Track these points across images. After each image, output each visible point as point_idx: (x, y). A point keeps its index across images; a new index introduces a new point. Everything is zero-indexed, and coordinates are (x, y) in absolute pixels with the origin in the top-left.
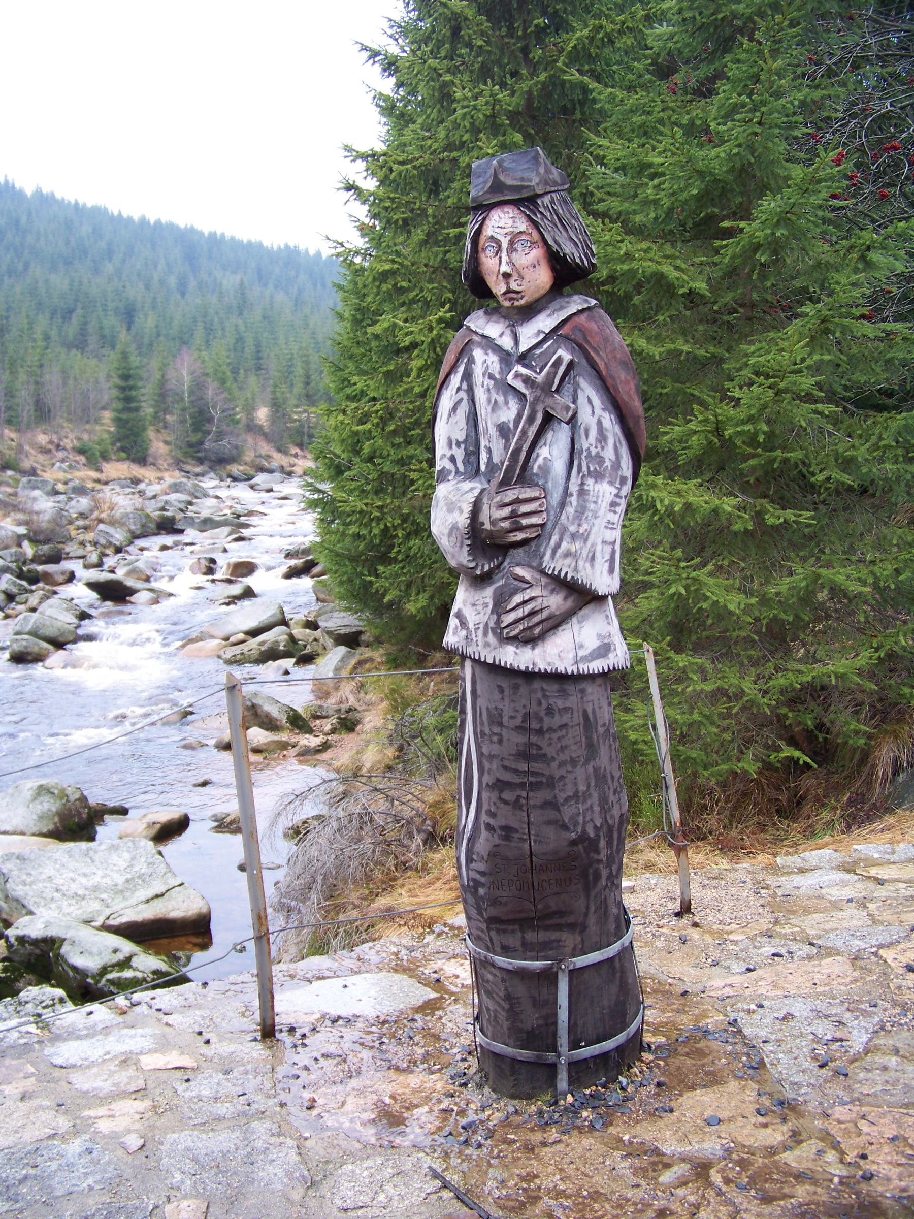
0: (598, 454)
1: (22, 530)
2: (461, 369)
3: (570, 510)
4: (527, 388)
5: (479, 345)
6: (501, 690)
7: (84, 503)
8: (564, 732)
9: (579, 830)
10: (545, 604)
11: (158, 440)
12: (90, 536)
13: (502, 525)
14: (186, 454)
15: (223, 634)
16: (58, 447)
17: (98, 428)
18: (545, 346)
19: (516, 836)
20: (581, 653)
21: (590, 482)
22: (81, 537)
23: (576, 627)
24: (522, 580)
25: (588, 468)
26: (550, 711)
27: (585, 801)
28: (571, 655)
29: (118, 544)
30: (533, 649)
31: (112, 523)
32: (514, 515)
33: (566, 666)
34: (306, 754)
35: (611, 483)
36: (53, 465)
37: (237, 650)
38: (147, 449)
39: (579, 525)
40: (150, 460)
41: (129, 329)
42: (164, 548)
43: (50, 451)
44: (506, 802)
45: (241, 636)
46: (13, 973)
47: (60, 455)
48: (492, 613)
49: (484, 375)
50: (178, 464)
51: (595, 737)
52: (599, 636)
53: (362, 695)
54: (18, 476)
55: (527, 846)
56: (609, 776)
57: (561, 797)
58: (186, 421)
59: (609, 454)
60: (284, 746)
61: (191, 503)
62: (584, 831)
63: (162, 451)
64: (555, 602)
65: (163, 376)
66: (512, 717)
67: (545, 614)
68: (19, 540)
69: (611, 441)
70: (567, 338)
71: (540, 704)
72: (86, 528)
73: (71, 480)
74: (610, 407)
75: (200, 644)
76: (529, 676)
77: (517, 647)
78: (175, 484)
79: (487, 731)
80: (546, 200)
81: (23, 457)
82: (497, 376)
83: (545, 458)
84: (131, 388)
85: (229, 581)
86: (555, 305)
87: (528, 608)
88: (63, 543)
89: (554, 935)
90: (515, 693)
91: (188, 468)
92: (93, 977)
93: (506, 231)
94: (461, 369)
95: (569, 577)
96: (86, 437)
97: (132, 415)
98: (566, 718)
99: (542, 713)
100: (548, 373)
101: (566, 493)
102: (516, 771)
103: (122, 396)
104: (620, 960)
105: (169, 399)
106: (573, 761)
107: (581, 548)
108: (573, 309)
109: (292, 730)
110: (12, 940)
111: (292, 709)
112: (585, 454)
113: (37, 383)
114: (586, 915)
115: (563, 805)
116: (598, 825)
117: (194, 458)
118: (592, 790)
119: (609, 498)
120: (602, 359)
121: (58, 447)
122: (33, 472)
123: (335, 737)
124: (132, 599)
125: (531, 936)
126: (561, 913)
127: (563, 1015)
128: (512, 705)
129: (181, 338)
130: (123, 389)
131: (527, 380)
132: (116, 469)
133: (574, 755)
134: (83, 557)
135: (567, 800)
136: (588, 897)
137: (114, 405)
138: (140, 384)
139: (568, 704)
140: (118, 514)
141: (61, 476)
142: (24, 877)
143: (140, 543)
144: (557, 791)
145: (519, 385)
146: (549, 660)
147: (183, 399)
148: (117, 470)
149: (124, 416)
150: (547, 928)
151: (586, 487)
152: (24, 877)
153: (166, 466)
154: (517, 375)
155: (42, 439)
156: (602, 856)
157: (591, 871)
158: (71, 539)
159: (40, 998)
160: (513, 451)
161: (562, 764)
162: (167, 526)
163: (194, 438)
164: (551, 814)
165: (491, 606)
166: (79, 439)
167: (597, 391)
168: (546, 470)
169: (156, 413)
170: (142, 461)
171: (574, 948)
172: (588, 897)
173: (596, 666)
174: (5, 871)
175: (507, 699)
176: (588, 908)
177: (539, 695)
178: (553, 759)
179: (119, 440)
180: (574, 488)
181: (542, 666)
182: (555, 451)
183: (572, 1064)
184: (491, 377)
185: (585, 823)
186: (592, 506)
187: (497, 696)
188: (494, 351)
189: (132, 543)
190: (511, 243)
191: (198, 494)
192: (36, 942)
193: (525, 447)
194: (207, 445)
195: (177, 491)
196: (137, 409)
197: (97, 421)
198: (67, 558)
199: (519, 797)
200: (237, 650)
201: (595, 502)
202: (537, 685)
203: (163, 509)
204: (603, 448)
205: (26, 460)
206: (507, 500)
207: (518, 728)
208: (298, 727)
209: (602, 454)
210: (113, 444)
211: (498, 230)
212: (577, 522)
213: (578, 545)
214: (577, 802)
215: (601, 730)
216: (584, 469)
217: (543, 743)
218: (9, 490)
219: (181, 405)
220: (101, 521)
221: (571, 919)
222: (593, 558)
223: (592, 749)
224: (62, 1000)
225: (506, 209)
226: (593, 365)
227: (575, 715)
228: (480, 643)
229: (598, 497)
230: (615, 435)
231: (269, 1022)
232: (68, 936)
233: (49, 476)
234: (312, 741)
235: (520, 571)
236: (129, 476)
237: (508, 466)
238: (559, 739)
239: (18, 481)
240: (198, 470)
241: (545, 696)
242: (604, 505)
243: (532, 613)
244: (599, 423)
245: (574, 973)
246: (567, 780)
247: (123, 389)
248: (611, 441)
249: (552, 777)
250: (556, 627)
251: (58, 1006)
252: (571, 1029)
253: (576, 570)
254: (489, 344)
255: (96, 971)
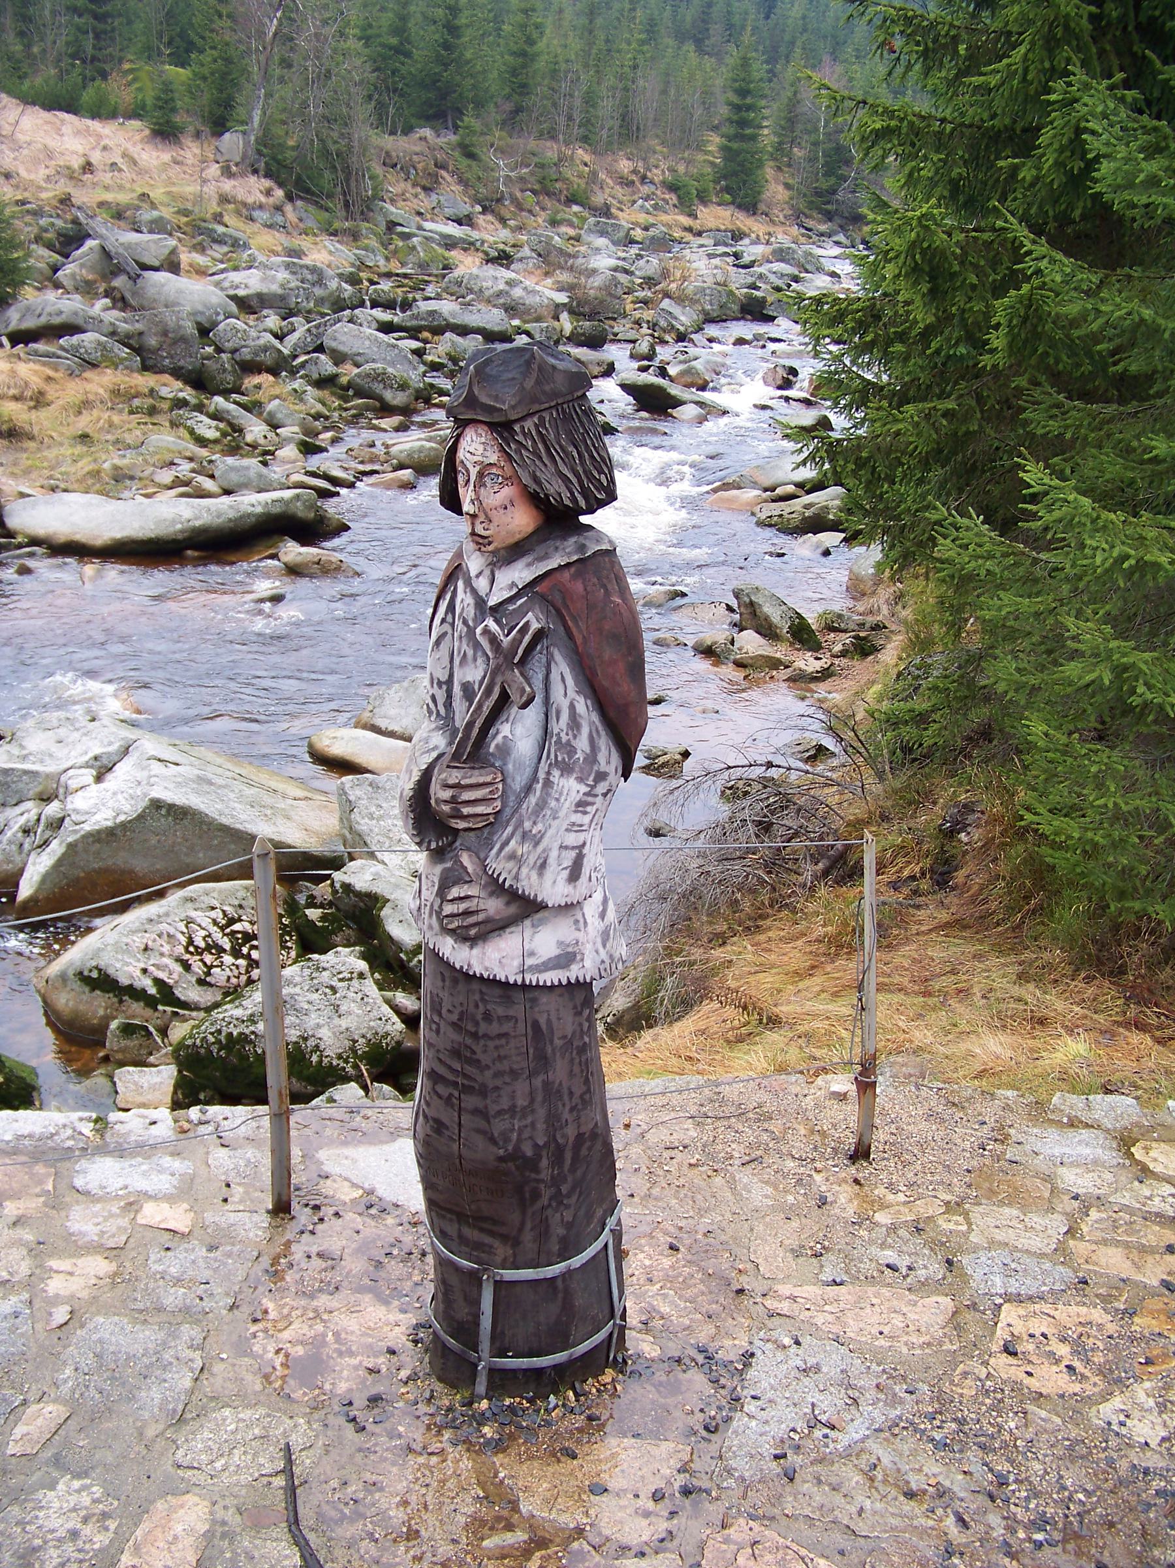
0: (568, 743)
1: (562, 298)
2: (448, 596)
3: (533, 800)
7: (651, 264)
8: (503, 1041)
9: (510, 1148)
10: (482, 906)
11: (777, 181)
12: (648, 315)
14: (811, 205)
15: (768, 483)
16: (643, 178)
17: (700, 157)
18: (519, 602)
20: (530, 962)
21: (556, 773)
22: (637, 314)
23: (528, 933)
26: (487, 1017)
27: (524, 1116)
28: (516, 963)
29: (682, 329)
30: (471, 948)
31: (681, 299)
32: (453, 800)
33: (508, 972)
34: (800, 680)
35: (580, 780)
36: (635, 202)
37: (776, 509)
38: (759, 193)
40: (762, 207)
41: (767, 17)
42: (740, 342)
43: (633, 182)
44: (440, 1097)
45: (791, 489)
46: (332, 923)
47: (646, 189)
50: (797, 217)
51: (549, 1050)
52: (560, 943)
53: (899, 607)
54: (586, 214)
55: (455, 1146)
56: (565, 1091)
57: (493, 1108)
58: (817, 159)
59: (582, 744)
60: (775, 664)
61: (796, 279)
62: (517, 1148)
63: (780, 197)
64: (493, 906)
65: (795, 93)
67: (481, 917)
68: (557, 309)
69: (585, 731)
70: (544, 598)
71: (477, 1006)
72: (645, 302)
73: (653, 225)
74: (588, 690)
75: (734, 493)
76: (466, 977)
78: (781, 250)
80: (529, 424)
81: (596, 188)
83: (505, 737)
84: (749, 108)
85: (807, 403)
86: (540, 550)
87: (463, 906)
88: (614, 319)
89: (487, 1239)
91: (810, 223)
92: (407, 953)
93: (476, 458)
94: (448, 596)
95: (507, 885)
96: (681, 168)
97: (744, 146)
98: (507, 1027)
99: (479, 1017)
100: (514, 639)
101: (534, 779)
102: (450, 1068)
103: (735, 118)
104: (564, 1281)
105: (800, 127)
106: (515, 1074)
107: (529, 853)
108: (553, 563)
109: (792, 644)
110: (338, 885)
111: (799, 616)
113: (626, 89)
114: (521, 1229)
115: (495, 1117)
116: (541, 1143)
117: (820, 211)
118: (536, 1105)
119: (575, 797)
120: (580, 631)
121: (643, 178)
122: (605, 211)
123: (844, 662)
124: (674, 412)
125: (467, 1232)
126: (495, 1222)
127: (486, 1322)
129: (834, 37)
130: (737, 108)
131: (493, 640)
132: (715, 216)
133: (515, 1066)
134: (634, 342)
135: (500, 1113)
136: (524, 1213)
137: (724, 130)
138: (763, 103)
139: (511, 1013)
140: (690, 287)
141: (642, 218)
142: (373, 809)
143: (712, 330)
144: (488, 1101)
146: (487, 964)
147: (816, 129)
148: (717, 217)
149: (735, 145)
150: (482, 1230)
152: (373, 809)
153: (782, 218)
154: (486, 631)
155: (625, 166)
156: (545, 1174)
157: (527, 1189)
158: (625, 315)
159: (339, 967)
161: (497, 1075)
162: (755, 311)
163: (824, 184)
164: (482, 1124)
166: (672, 170)
167: (572, 670)
168: (505, 750)
169: (780, 143)
170: (750, 206)
171: (505, 1260)
172: (524, 1213)
173: (550, 977)
174: (352, 798)
176: (523, 1223)
177: (477, 997)
178: (488, 1067)
179: (725, 177)
180: (541, 775)
181: (478, 969)
182: (519, 730)
183: (493, 1371)
185: (519, 1140)
186: (553, 804)
189: (700, 329)
190: (481, 475)
191: (808, 267)
192: (359, 894)
193: (478, 725)
194: (840, 196)
195: (782, 260)
196: (753, 138)
197: (700, 147)
198: (613, 341)
199: (451, 1095)
200: (776, 509)
201: (557, 800)
202: (475, 986)
203: (754, 287)
204: (575, 737)
205: (599, 192)
206: (451, 782)
207: (454, 1024)
208: (801, 642)
209: (573, 743)
210: (716, 182)
213: (527, 847)
214: (513, 1117)
215: (558, 1043)
217: (478, 1049)
218: (572, 232)
219: (813, 137)
220: (667, 295)
221: (503, 1230)
222: (543, 865)
223: (543, 1061)
224: (361, 976)
226: (570, 636)
227: (521, 1026)
229: (561, 794)
230: (591, 723)
231: (285, 1198)
232: (392, 897)
233: (625, 218)
234: (808, 663)
236: (730, 227)
238: (496, 1048)
239: (585, 220)
240: (823, 228)
241: (482, 999)
242: (568, 804)
243: (467, 913)
244: (572, 707)
245: (499, 1285)
246: (502, 1092)
247: (737, 108)
248: (585, 731)
249: (484, 1085)
250: (503, 928)
251: (355, 983)
252: (494, 1337)
253: (517, 878)
255: (410, 947)
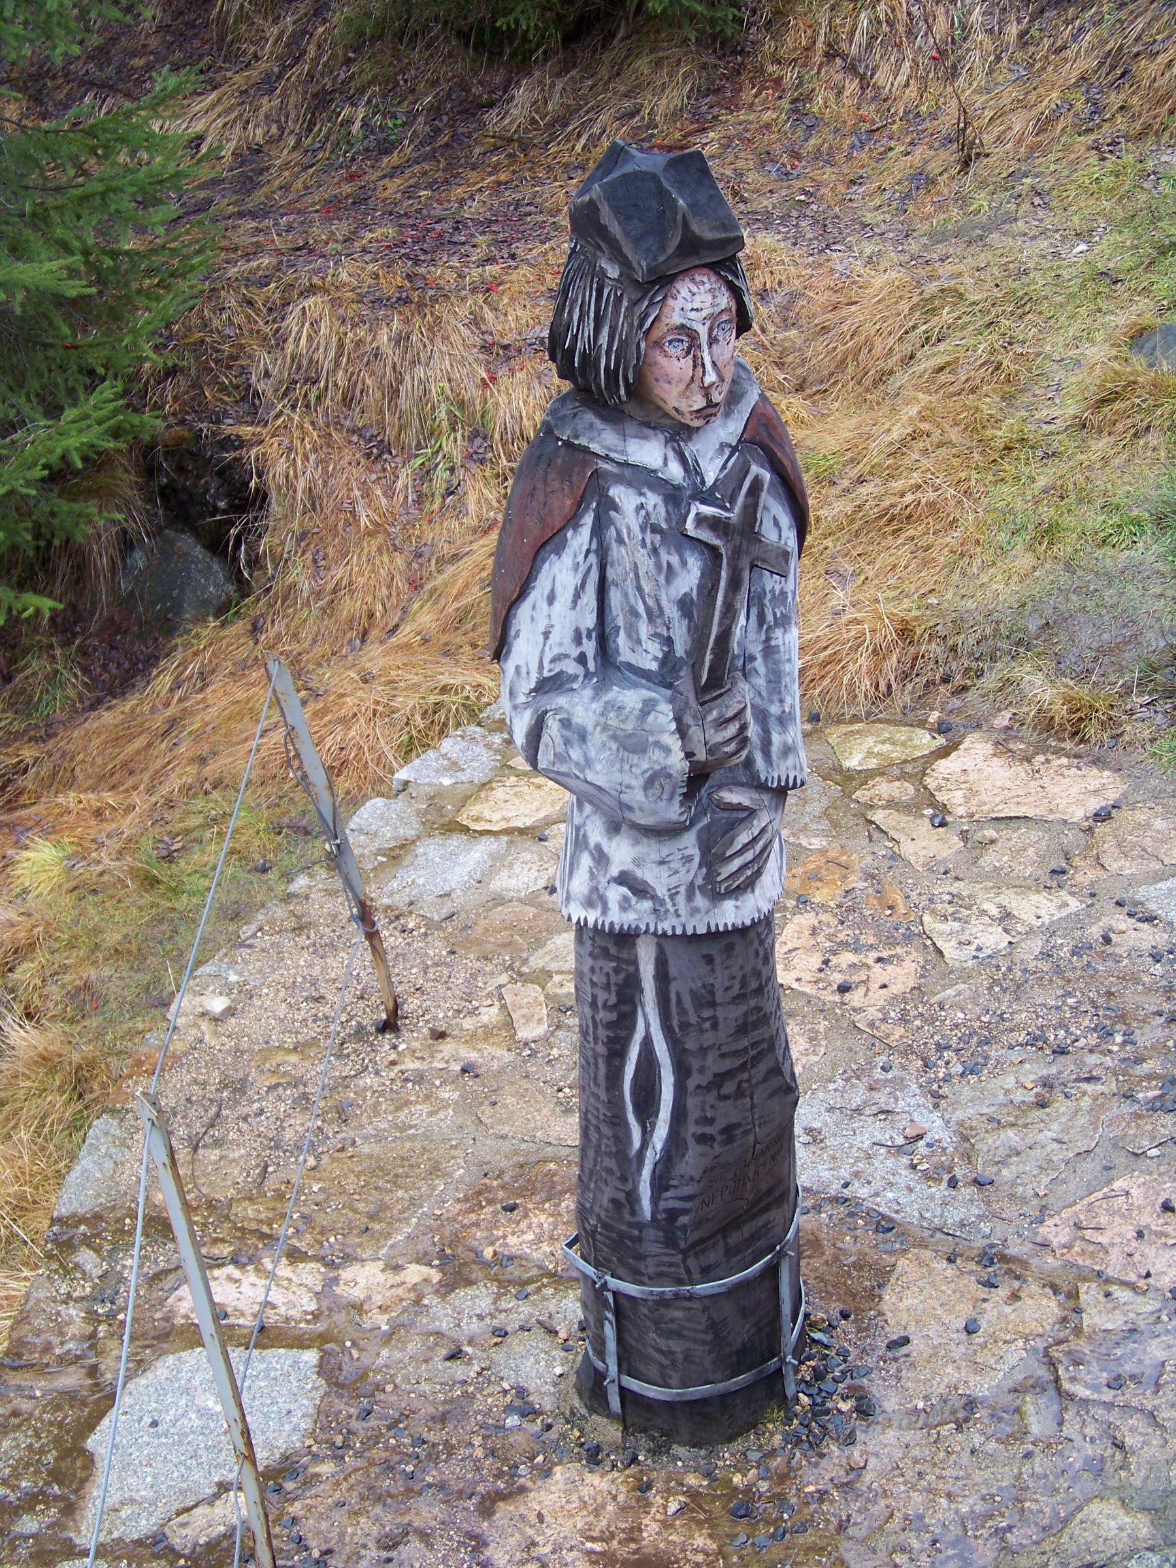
4: (718, 537)
5: (619, 479)
6: (709, 959)
13: (727, 749)
19: (738, 1132)
24: (739, 808)
25: (775, 614)
30: (753, 891)
39: (781, 701)
48: (700, 867)
49: (643, 529)
66: (727, 989)
77: (737, 899)
79: (693, 1019)
82: (664, 526)
89: (760, 1221)
90: (729, 957)
93: (704, 313)
100: (745, 507)
112: (769, 596)
128: (726, 972)
131: (714, 524)
145: (706, 536)
151: (773, 643)
154: (700, 520)
160: (718, 638)
165: (697, 859)
175: (718, 969)
184: (655, 529)
187: (703, 968)
188: (651, 488)
211: (693, 315)
212: (775, 697)
216: (770, 618)
225: (698, 278)
228: (682, 912)
235: (733, 797)
237: (712, 662)
254: (642, 477)
